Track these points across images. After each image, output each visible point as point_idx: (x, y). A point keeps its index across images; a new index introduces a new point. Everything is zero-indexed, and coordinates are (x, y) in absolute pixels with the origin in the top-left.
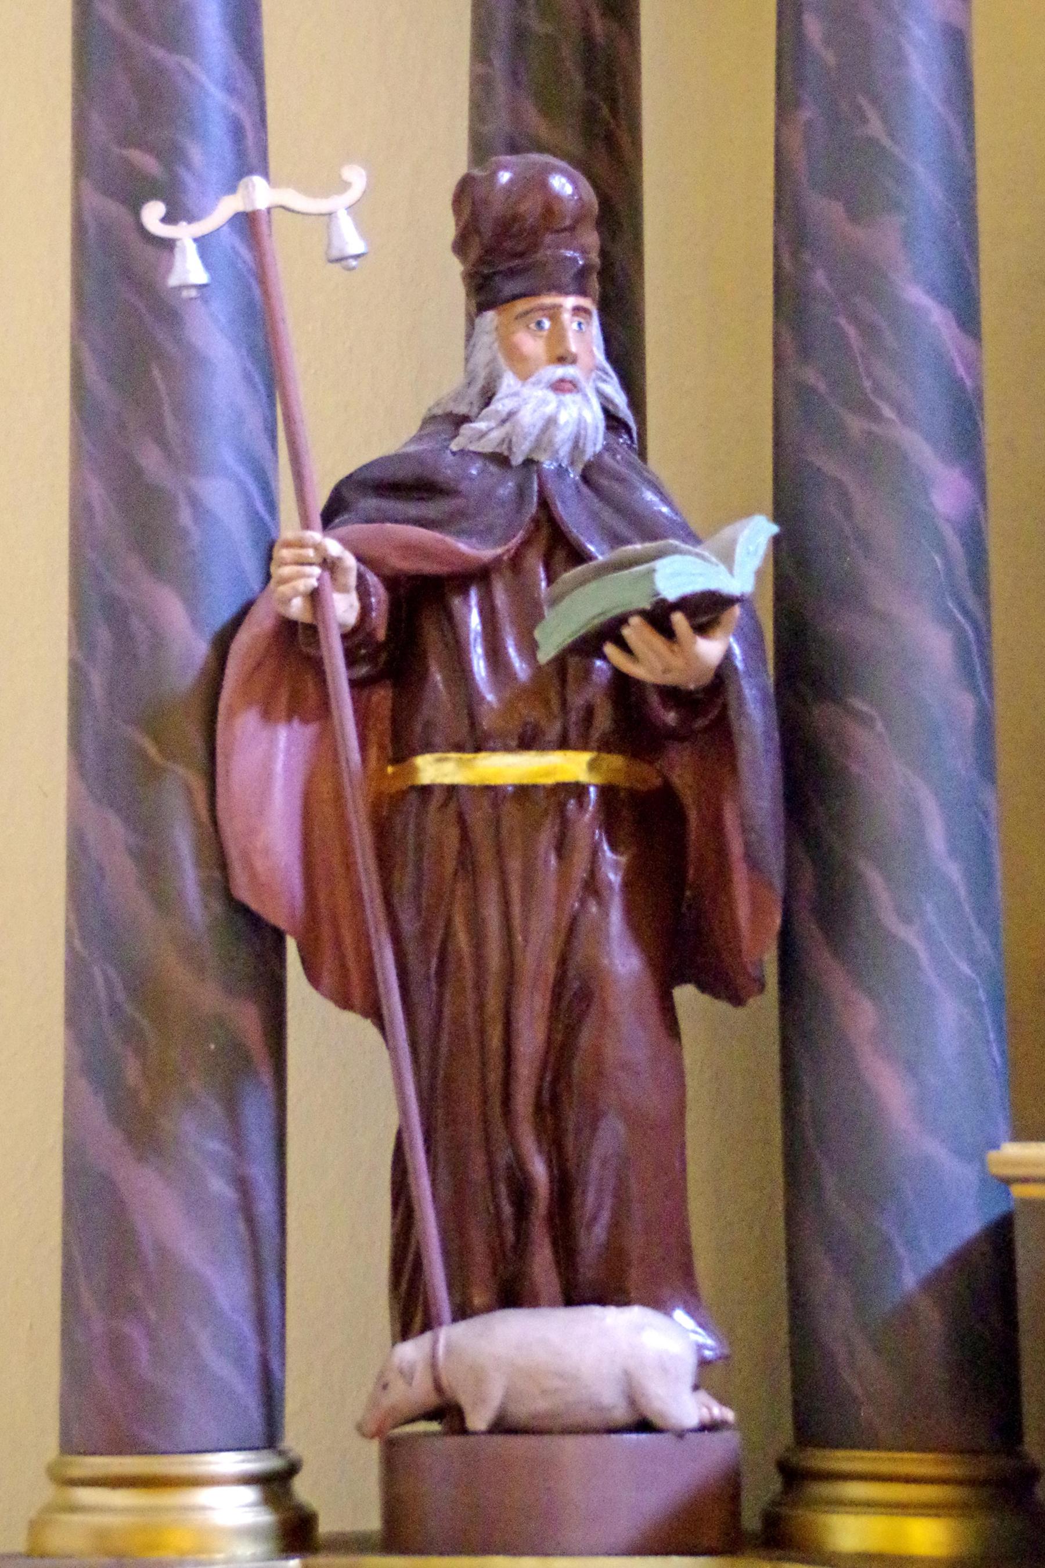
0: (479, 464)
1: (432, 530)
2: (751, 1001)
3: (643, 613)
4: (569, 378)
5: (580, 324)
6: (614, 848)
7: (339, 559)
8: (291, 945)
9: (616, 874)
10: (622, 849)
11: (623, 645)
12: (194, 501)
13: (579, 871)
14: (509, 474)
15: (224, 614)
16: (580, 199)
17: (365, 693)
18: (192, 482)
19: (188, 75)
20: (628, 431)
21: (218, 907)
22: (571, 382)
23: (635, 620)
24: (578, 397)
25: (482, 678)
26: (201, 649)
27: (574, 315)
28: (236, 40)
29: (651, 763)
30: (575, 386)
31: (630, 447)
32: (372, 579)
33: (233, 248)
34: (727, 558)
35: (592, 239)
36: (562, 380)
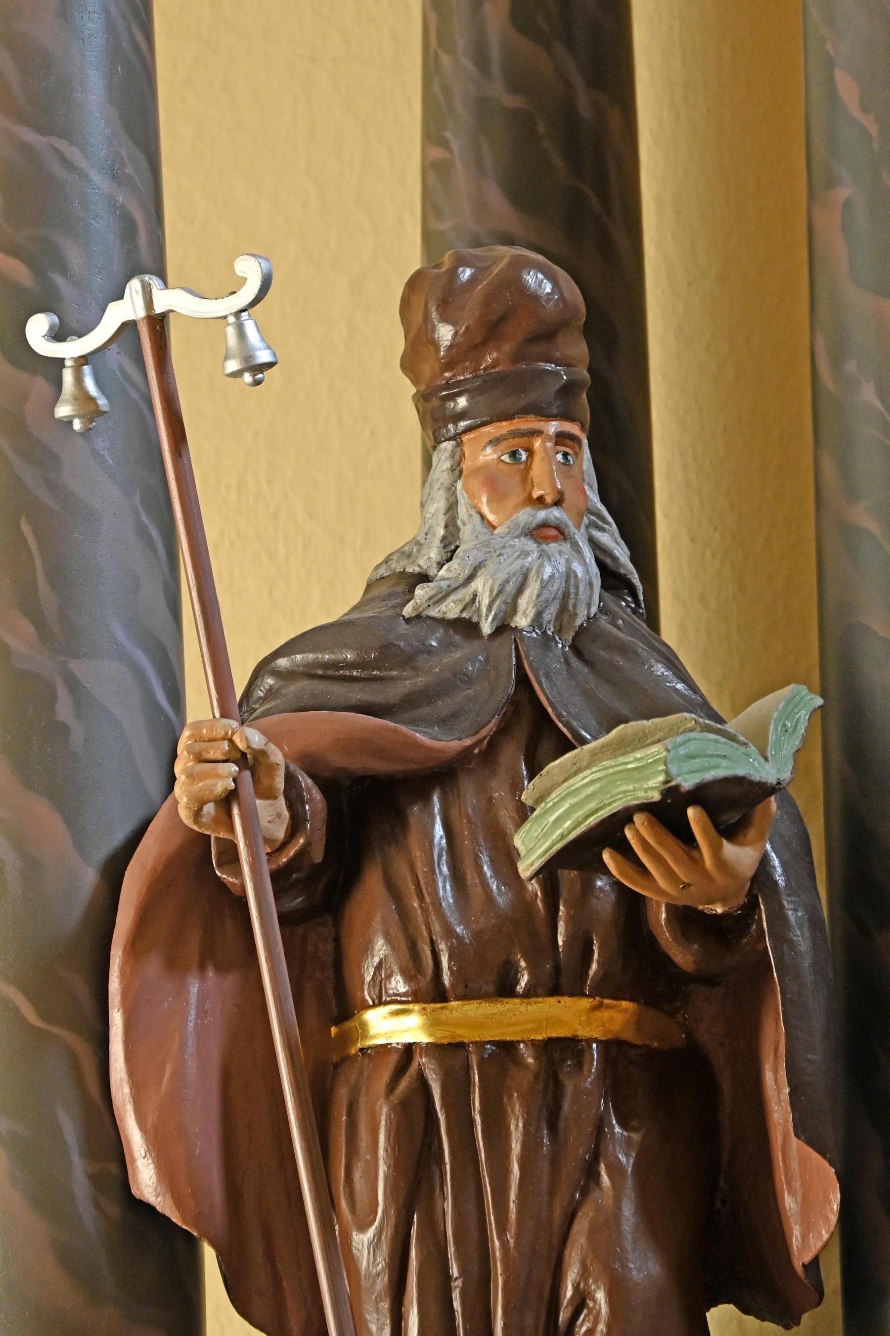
0: (440, 632)
1: (385, 719)
2: (805, 1317)
3: (646, 808)
4: (554, 522)
5: (565, 455)
6: (623, 1124)
7: (263, 753)
8: (209, 1256)
9: (627, 1156)
10: (635, 1123)
11: (624, 849)
12: (74, 685)
13: (577, 1151)
14: (476, 645)
15: (119, 836)
16: (562, 298)
17: (300, 931)
18: (76, 667)
19: (69, 166)
20: (633, 592)
21: (114, 1210)
22: (557, 528)
23: (639, 819)
24: (566, 547)
25: (449, 905)
26: (89, 878)
27: (557, 444)
28: (128, 127)
29: (671, 1014)
30: (562, 533)
31: (634, 611)
32: (306, 781)
33: (122, 370)
34: (759, 740)
35: (577, 349)
36: (544, 525)
